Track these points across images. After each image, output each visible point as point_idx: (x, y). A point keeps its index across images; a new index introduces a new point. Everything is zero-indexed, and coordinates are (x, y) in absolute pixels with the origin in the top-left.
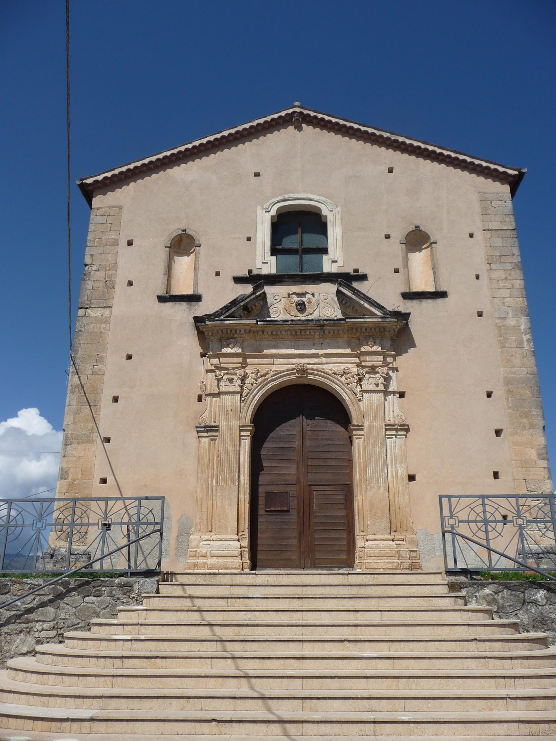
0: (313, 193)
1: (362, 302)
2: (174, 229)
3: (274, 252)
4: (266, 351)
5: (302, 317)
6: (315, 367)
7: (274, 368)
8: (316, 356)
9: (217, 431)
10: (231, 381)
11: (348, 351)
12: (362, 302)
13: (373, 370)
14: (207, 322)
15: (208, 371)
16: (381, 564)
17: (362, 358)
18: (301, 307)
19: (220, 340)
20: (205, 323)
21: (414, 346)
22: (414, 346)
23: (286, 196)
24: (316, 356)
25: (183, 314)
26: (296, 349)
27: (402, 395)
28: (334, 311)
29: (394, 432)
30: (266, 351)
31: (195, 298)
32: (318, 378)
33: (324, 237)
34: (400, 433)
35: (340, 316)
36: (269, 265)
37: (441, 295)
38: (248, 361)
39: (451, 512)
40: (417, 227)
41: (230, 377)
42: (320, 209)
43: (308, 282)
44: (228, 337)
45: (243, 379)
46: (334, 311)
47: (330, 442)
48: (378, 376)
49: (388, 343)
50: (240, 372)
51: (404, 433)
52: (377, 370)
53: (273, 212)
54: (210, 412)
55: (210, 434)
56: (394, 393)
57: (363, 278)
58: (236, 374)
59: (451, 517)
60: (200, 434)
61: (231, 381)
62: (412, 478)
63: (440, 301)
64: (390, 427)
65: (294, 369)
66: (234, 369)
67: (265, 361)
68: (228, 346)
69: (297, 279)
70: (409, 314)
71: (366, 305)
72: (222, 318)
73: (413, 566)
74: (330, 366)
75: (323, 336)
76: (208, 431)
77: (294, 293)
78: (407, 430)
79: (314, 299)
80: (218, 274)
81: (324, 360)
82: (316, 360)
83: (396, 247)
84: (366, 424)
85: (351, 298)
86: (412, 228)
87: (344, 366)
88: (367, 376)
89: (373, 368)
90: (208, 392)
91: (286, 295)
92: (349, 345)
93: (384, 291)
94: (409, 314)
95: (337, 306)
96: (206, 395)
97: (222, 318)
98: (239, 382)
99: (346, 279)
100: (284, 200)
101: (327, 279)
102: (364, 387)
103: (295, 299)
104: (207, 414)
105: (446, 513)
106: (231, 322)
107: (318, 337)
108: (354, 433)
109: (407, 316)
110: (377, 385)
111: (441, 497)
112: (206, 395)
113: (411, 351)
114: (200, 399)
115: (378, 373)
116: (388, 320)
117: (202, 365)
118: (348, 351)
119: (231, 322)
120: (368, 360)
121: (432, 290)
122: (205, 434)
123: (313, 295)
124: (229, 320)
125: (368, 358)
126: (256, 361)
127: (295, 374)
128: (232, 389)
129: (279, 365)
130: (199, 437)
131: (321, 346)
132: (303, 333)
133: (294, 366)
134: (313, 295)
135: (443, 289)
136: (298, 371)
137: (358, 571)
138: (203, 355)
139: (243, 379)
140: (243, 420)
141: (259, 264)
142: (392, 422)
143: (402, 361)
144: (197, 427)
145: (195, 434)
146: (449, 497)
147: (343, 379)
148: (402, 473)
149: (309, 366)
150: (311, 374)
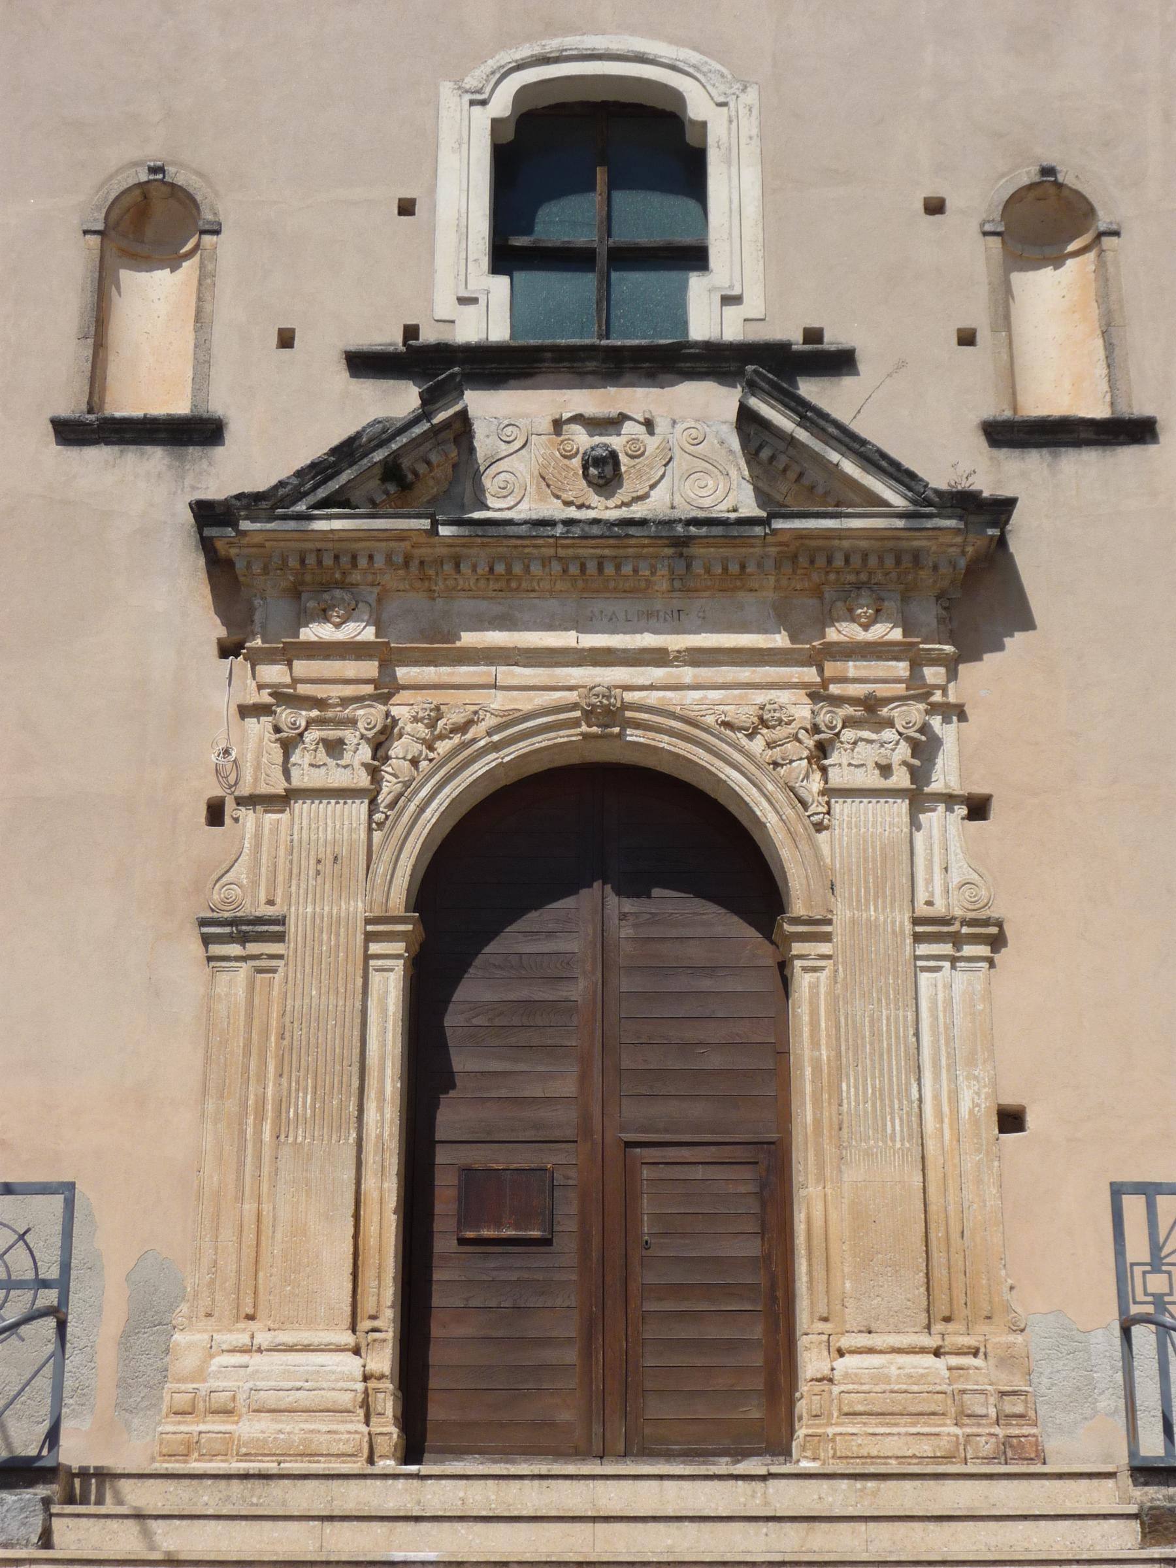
0: (652, 32)
1: (834, 457)
2: (119, 162)
3: (504, 259)
4: (469, 639)
5: (605, 509)
6: (653, 698)
7: (498, 701)
8: (659, 658)
9: (280, 937)
10: (334, 748)
11: (780, 640)
12: (834, 457)
13: (871, 711)
14: (245, 525)
15: (245, 711)
16: (894, 1443)
17: (832, 668)
18: (604, 471)
19: (295, 592)
20: (234, 525)
21: (1026, 622)
22: (1026, 622)
23: (552, 45)
24: (659, 658)
25: (150, 493)
26: (582, 628)
27: (978, 808)
28: (730, 492)
29: (947, 949)
30: (469, 639)
31: (197, 432)
32: (664, 742)
33: (692, 204)
34: (968, 950)
35: (750, 508)
36: (482, 309)
37: (1134, 431)
38: (403, 673)
39: (1156, 1247)
40: (1048, 171)
41: (332, 734)
42: (678, 97)
43: (628, 377)
44: (323, 581)
45: (380, 744)
46: (730, 492)
47: (706, 984)
48: (888, 734)
49: (928, 613)
50: (370, 716)
51: (983, 950)
52: (884, 712)
53: (502, 104)
54: (258, 860)
55: (253, 948)
56: (950, 800)
57: (841, 362)
58: (353, 722)
59: (1156, 1264)
60: (216, 949)
61: (334, 748)
62: (1011, 1120)
63: (1128, 455)
64: (931, 928)
65: (575, 706)
66: (345, 702)
67: (463, 674)
68: (323, 615)
69: (591, 365)
70: (1011, 503)
71: (850, 468)
72: (301, 507)
73: (1008, 1448)
74: (708, 695)
75: (684, 585)
76: (244, 939)
77: (578, 419)
78: (997, 942)
79: (652, 443)
80: (286, 340)
81: (688, 674)
82: (657, 674)
83: (964, 249)
84: (842, 914)
85: (791, 440)
86: (1027, 175)
87: (760, 697)
88: (848, 735)
89: (871, 704)
90: (245, 790)
91: (546, 425)
92: (782, 618)
93: (917, 416)
94: (1011, 503)
95: (739, 469)
96: (240, 801)
97: (301, 507)
98: (365, 753)
99: (777, 367)
100: (545, 60)
101: (702, 366)
102: (837, 778)
103: (582, 439)
104: (240, 873)
105: (1137, 1248)
106: (337, 524)
107: (665, 586)
108: (797, 948)
109: (1002, 508)
110: (885, 770)
111: (1117, 1191)
112: (240, 801)
113: (1016, 642)
114: (215, 814)
115: (890, 723)
116: (929, 524)
117: (228, 686)
118: (780, 640)
119: (337, 524)
120: (852, 673)
121: (1099, 411)
122: (235, 949)
123: (649, 424)
124: (329, 517)
125: (852, 668)
126: (429, 674)
127: (575, 723)
128: (338, 778)
129: (517, 689)
130: (210, 959)
131: (676, 622)
132: (609, 570)
133: (572, 697)
134: (649, 424)
135: (1141, 408)
136: (589, 715)
137: (806, 1465)
138: (227, 650)
139: (380, 744)
140: (379, 897)
141: (444, 306)
142: (939, 909)
143: (978, 680)
144: (203, 922)
145: (196, 948)
146: (1150, 1191)
147: (757, 745)
148: (976, 1101)
149: (630, 697)
150: (638, 725)
